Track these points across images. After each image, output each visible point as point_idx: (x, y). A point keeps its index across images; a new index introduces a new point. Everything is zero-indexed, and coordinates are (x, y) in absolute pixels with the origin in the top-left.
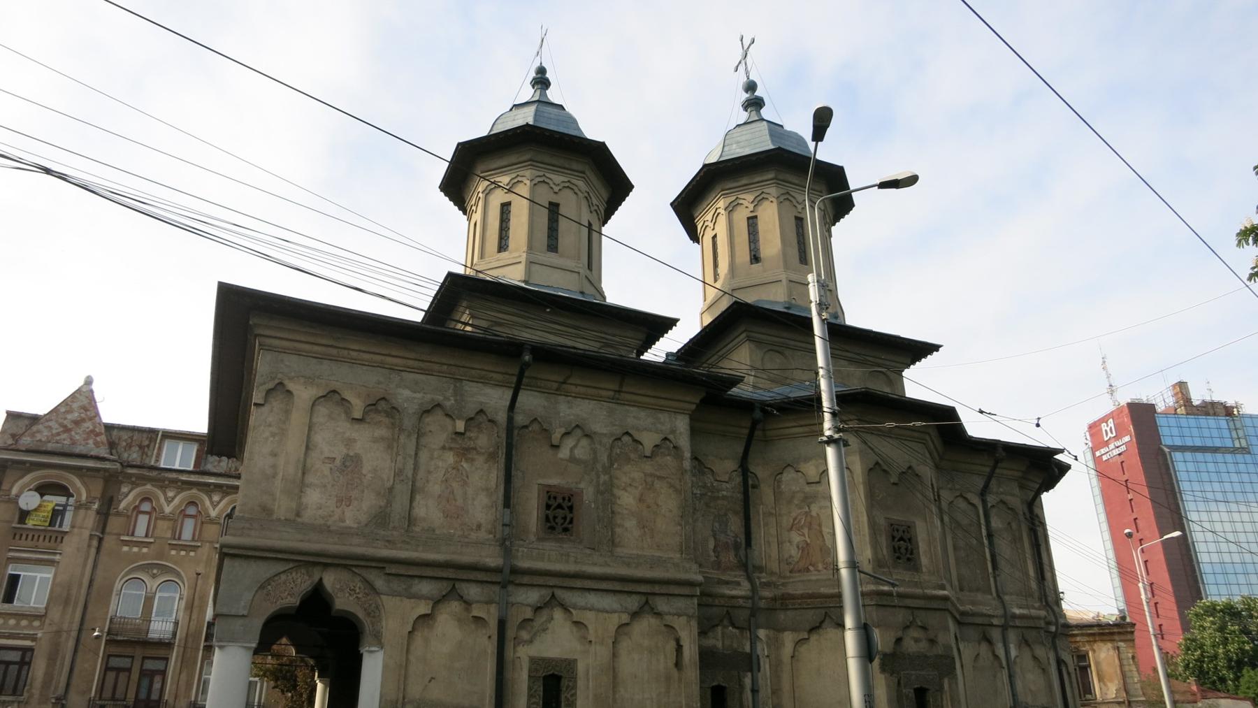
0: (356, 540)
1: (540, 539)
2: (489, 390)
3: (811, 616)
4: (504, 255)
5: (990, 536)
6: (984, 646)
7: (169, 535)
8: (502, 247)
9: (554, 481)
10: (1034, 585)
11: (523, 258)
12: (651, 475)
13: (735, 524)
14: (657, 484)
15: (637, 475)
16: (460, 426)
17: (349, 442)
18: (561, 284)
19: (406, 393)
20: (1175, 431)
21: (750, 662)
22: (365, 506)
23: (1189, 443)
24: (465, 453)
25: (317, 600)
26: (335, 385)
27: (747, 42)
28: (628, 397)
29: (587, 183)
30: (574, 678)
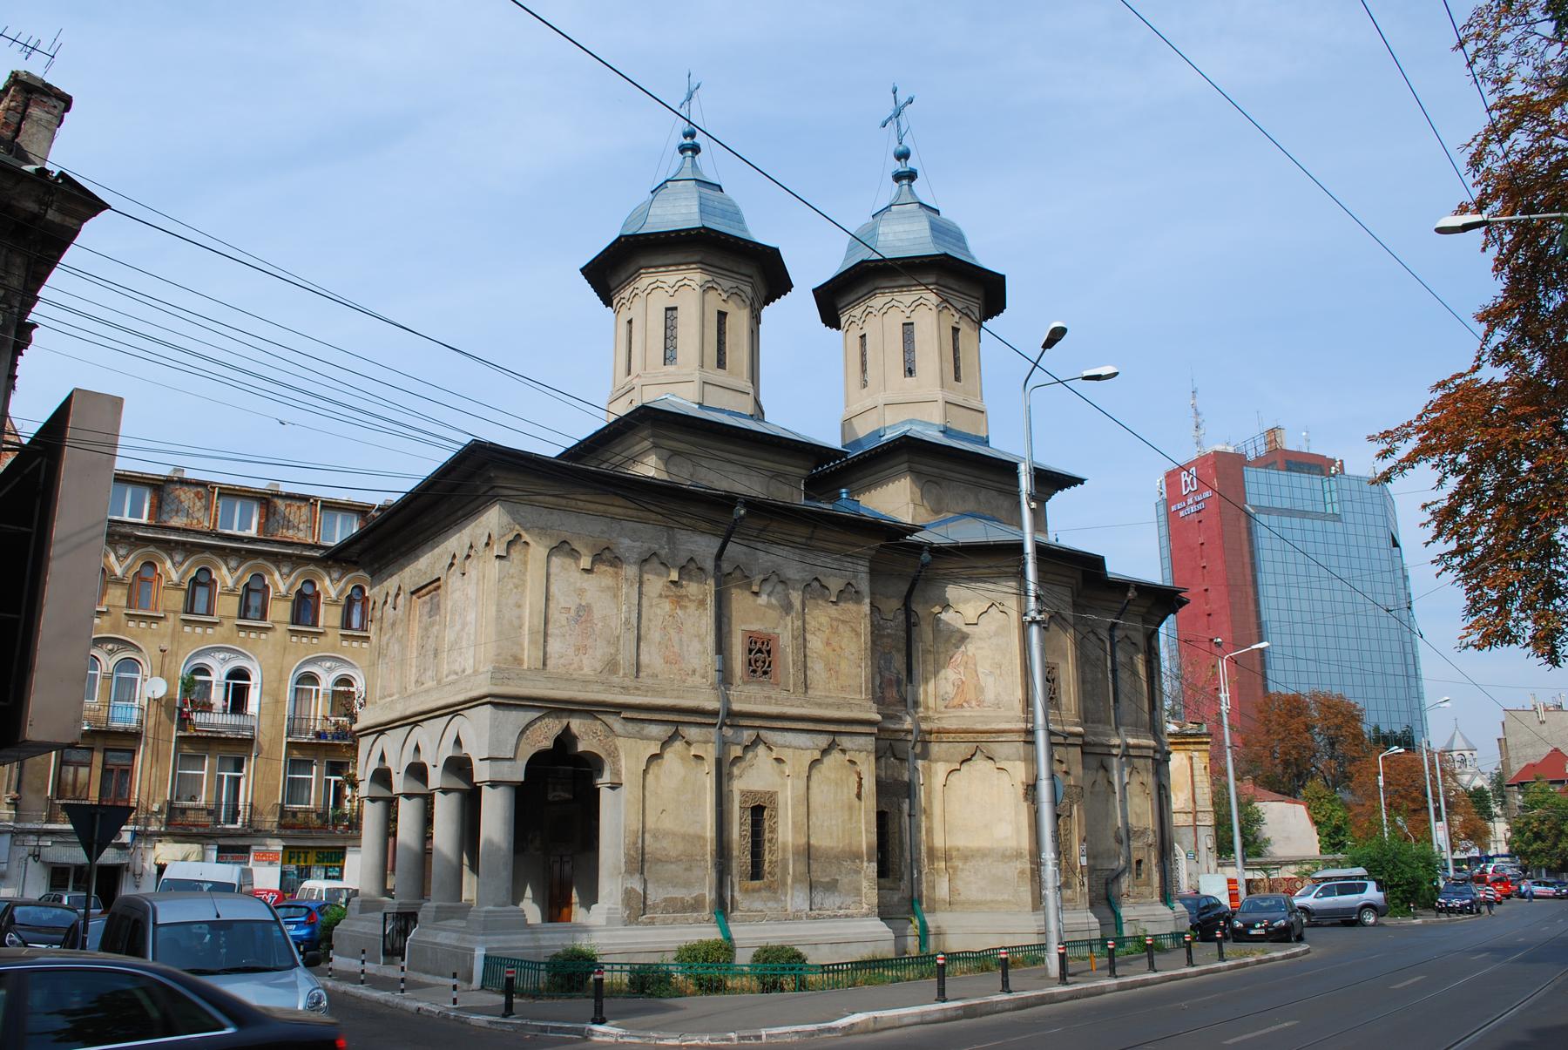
0: (596, 687)
1: (745, 683)
2: (698, 538)
3: (964, 749)
4: (670, 368)
5: (1114, 671)
6: (1101, 772)
7: (124, 603)
8: (669, 358)
9: (755, 627)
10: (1147, 717)
11: (696, 376)
12: (837, 620)
13: (899, 661)
14: (841, 626)
15: (824, 620)
16: (674, 576)
17: (581, 592)
18: (728, 408)
19: (627, 542)
20: (1264, 489)
21: (909, 790)
22: (598, 654)
23: (1277, 504)
24: (679, 601)
25: (565, 740)
26: (565, 535)
27: (902, 99)
28: (818, 544)
29: (753, 288)
30: (775, 809)
